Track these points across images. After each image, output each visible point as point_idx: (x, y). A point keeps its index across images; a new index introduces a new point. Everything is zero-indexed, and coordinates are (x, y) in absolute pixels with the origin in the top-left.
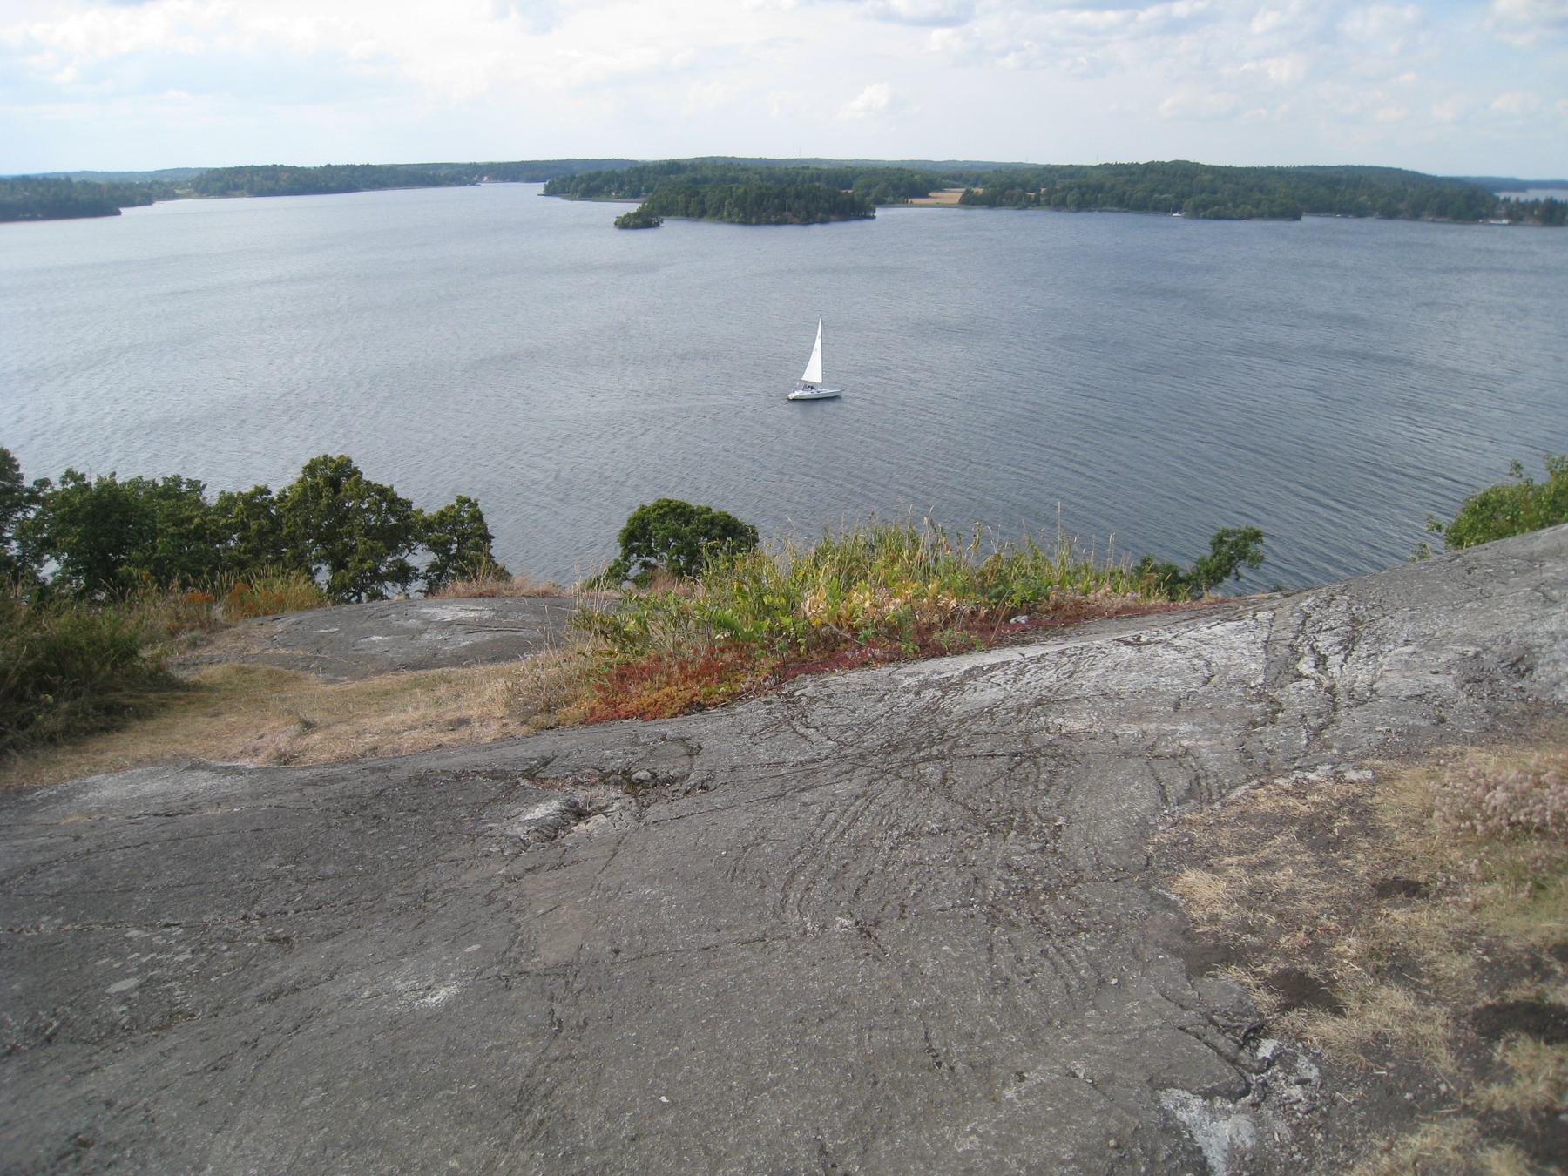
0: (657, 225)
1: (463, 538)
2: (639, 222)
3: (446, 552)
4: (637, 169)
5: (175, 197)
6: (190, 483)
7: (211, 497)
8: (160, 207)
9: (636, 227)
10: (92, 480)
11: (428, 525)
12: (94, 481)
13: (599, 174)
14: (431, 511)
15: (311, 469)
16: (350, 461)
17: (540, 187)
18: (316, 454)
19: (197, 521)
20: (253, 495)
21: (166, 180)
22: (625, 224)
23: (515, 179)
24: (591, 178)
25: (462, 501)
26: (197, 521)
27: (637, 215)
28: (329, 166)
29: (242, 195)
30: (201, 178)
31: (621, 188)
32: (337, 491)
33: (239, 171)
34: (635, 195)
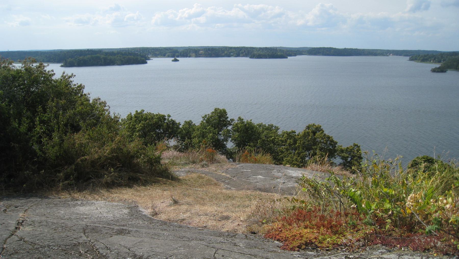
0: (445, 72)
1: (353, 157)
2: (439, 70)
3: (346, 160)
4: (441, 54)
7: (280, 132)
8: (298, 57)
9: (438, 72)
10: (245, 121)
11: (342, 151)
14: (344, 147)
15: (308, 127)
18: (311, 123)
19: (273, 137)
20: (290, 133)
21: (301, 50)
22: (434, 71)
23: (400, 55)
24: (425, 56)
26: (273, 137)
27: (439, 68)
28: (345, 48)
29: (320, 55)
31: (435, 59)
32: (315, 135)
33: (320, 48)
34: (439, 62)
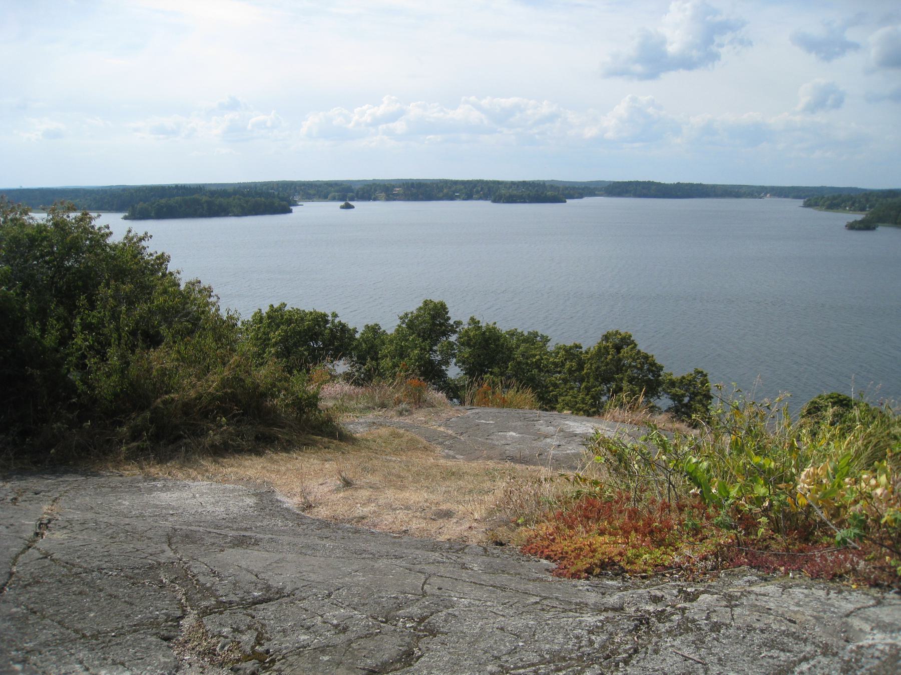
0: (874, 229)
2: (862, 226)
3: (680, 401)
5: (595, 195)
6: (542, 336)
7: (551, 347)
8: (586, 200)
9: (860, 229)
10: (483, 324)
11: (672, 384)
12: (484, 325)
13: (840, 196)
14: (676, 376)
15: (606, 338)
16: (630, 336)
17: (801, 202)
18: (612, 328)
19: (537, 357)
20: (571, 348)
21: (592, 187)
22: (852, 227)
23: (786, 196)
24: (834, 198)
25: (698, 372)
26: (537, 357)
27: (861, 222)
28: (678, 183)
30: (609, 186)
31: (853, 204)
32: (618, 352)
34: (862, 209)
